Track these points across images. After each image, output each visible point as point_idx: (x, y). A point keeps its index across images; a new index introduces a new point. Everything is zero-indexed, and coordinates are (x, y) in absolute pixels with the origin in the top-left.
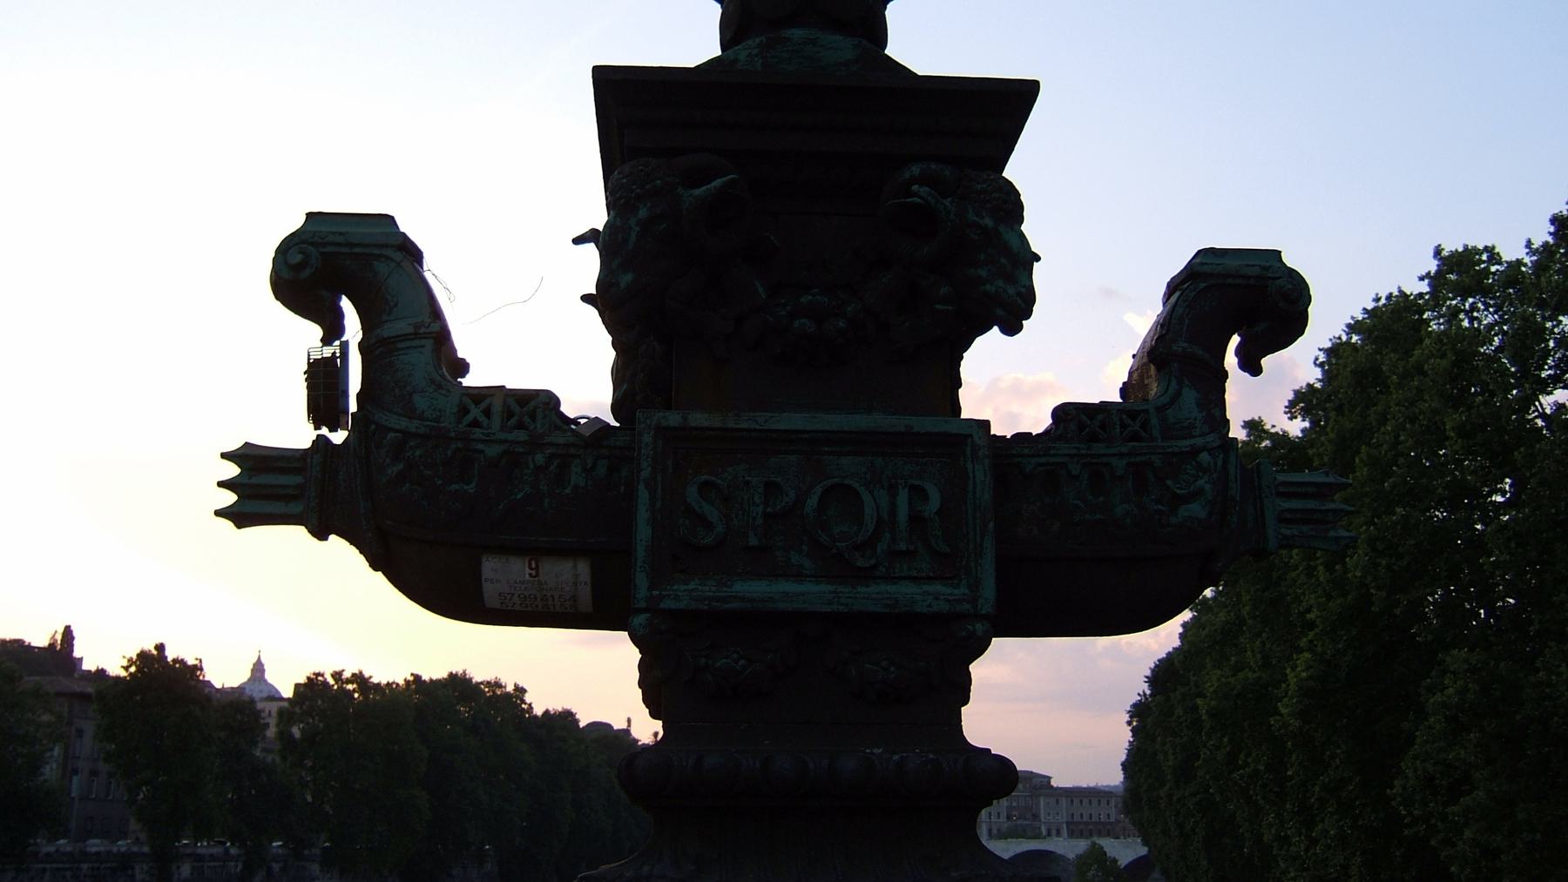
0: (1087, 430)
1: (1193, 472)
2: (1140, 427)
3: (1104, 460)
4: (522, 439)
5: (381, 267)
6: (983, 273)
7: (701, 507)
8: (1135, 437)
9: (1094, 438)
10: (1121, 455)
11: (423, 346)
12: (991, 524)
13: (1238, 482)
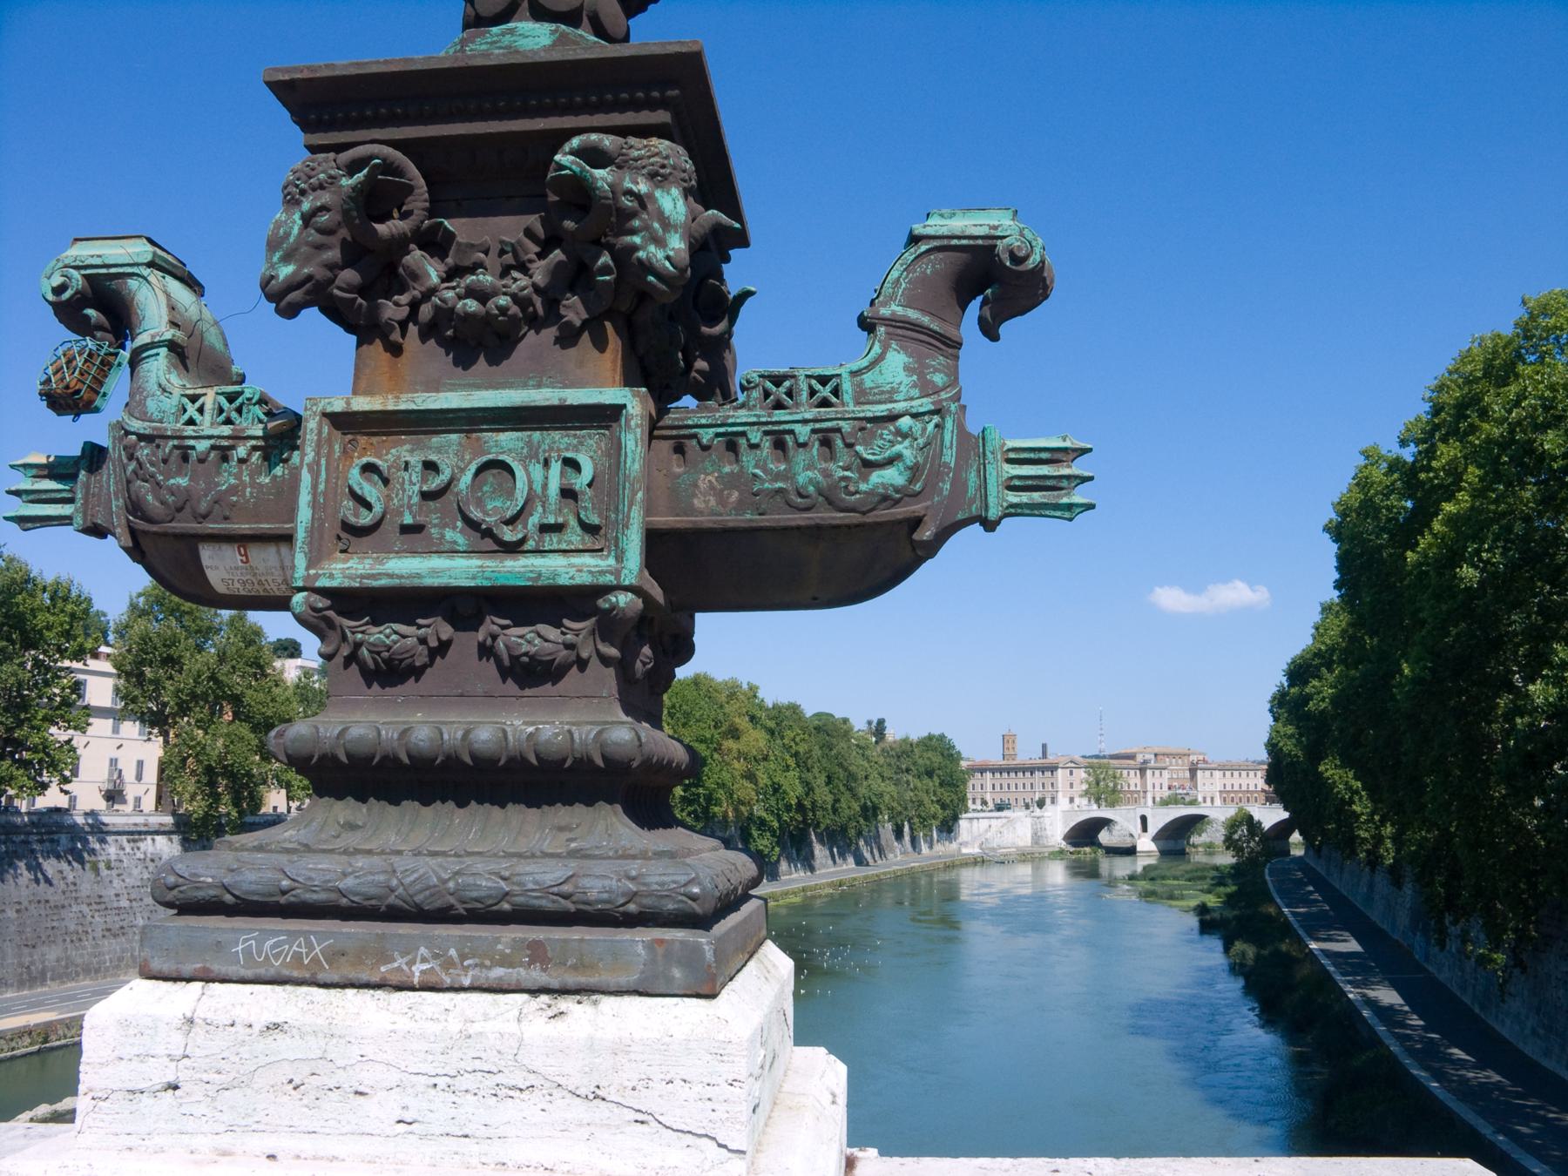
0: (772, 397)
1: (890, 437)
2: (831, 392)
3: (787, 427)
4: (225, 434)
5: (133, 283)
6: (637, 240)
7: (361, 488)
8: (825, 403)
9: (779, 405)
10: (805, 422)
11: (158, 354)
12: (640, 495)
13: (954, 449)
